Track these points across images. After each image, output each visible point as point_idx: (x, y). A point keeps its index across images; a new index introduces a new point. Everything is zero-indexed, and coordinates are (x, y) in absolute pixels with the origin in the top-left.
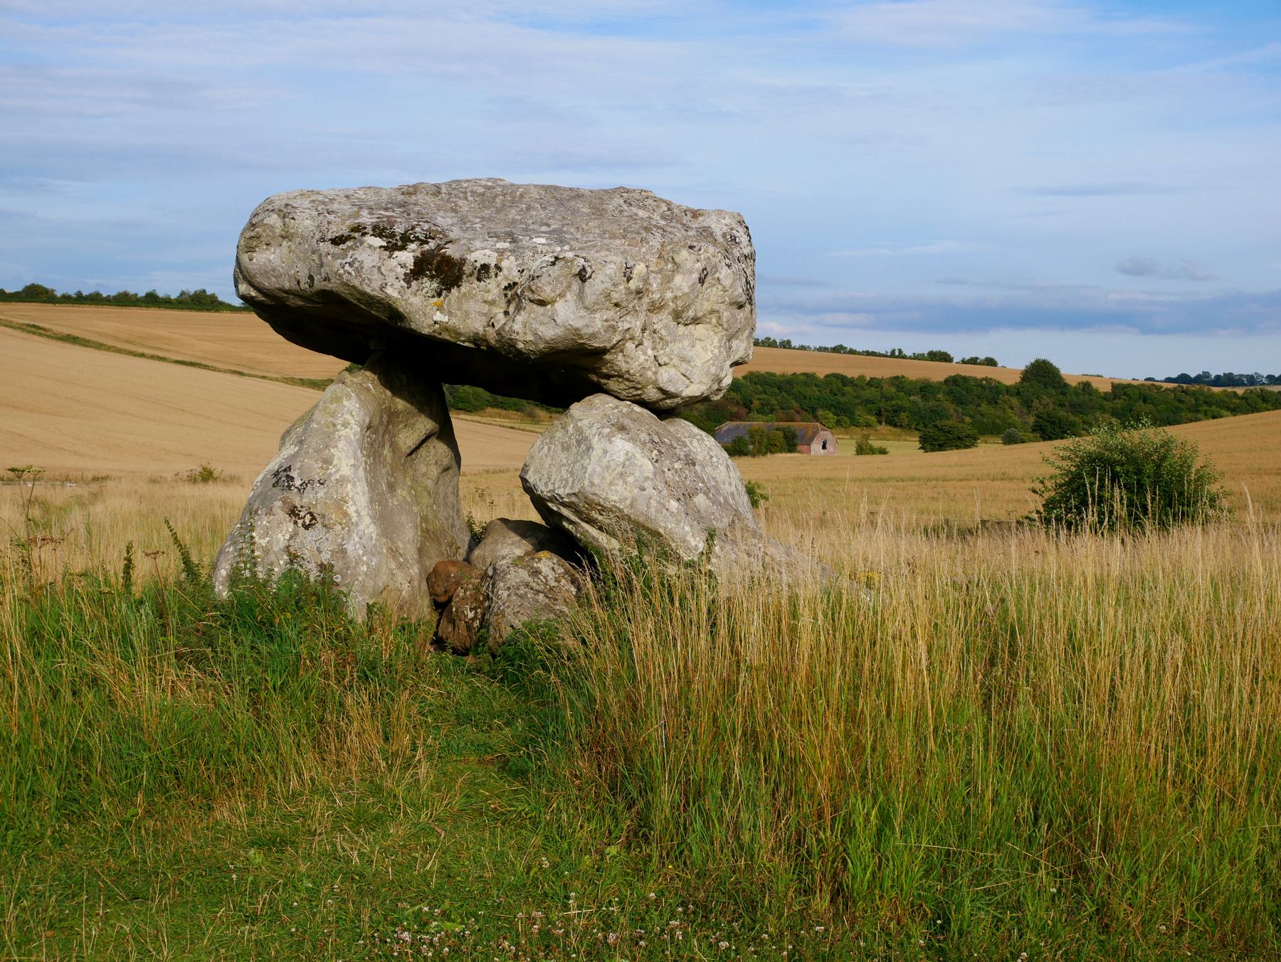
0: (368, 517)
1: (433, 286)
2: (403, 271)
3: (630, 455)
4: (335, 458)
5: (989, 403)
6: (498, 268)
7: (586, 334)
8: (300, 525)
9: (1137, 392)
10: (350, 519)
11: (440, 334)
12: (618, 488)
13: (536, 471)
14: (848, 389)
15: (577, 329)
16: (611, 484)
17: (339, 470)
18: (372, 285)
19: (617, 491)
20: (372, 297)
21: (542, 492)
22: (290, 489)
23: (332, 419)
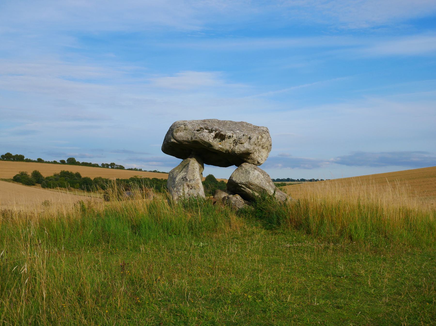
6: (233, 137)
13: (235, 178)
14: (158, 182)
15: (249, 149)
16: (255, 180)
20: (206, 142)
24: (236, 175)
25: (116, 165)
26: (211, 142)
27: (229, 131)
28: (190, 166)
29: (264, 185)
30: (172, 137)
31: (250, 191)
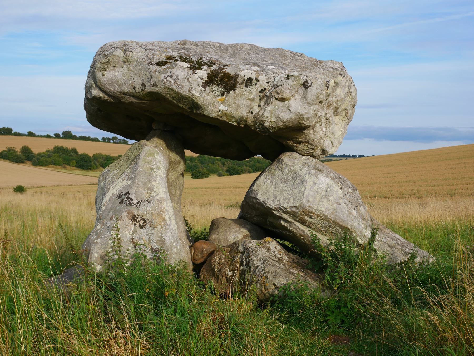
0: (174, 221)
2: (202, 81)
3: (329, 185)
4: (155, 187)
5: (212, 163)
6: (257, 80)
8: (137, 226)
9: (257, 160)
10: (166, 222)
11: (221, 117)
12: (324, 204)
13: (263, 194)
15: (302, 115)
16: (319, 201)
17: (158, 194)
19: (324, 205)
20: (182, 96)
21: (271, 205)
22: (131, 205)
23: (150, 166)
24: (267, 187)
25: (119, 139)
26: (197, 94)
27: (248, 66)
28: (141, 163)
30: (95, 83)
31: (307, 231)
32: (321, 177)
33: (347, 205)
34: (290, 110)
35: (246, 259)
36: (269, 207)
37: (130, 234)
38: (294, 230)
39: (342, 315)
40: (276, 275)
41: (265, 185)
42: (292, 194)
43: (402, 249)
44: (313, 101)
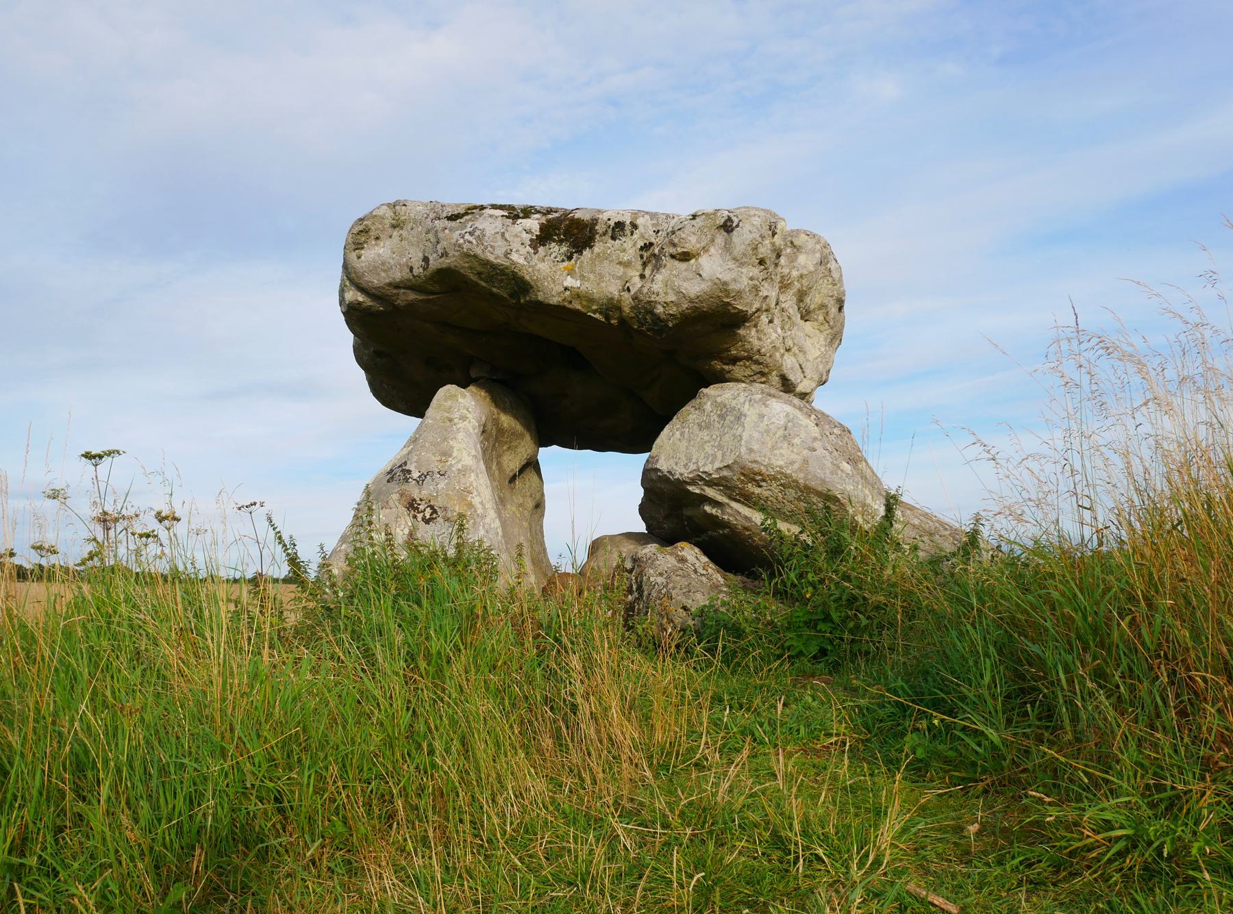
0: (493, 511)
1: (562, 251)
2: (529, 236)
3: (791, 416)
6: (634, 226)
7: (733, 290)
8: (419, 519)
10: (475, 511)
11: (570, 302)
12: (783, 452)
15: (725, 283)
18: (496, 252)
20: (494, 266)
21: (681, 474)
23: (447, 415)
24: (674, 444)
26: (521, 261)
29: (829, 477)
31: (758, 517)
32: (775, 403)
33: (831, 453)
34: (700, 275)
35: (636, 578)
36: (678, 479)
37: (404, 534)
38: (731, 519)
39: (822, 639)
40: (690, 591)
41: (671, 442)
42: (719, 445)
43: (954, 538)
44: (744, 254)
